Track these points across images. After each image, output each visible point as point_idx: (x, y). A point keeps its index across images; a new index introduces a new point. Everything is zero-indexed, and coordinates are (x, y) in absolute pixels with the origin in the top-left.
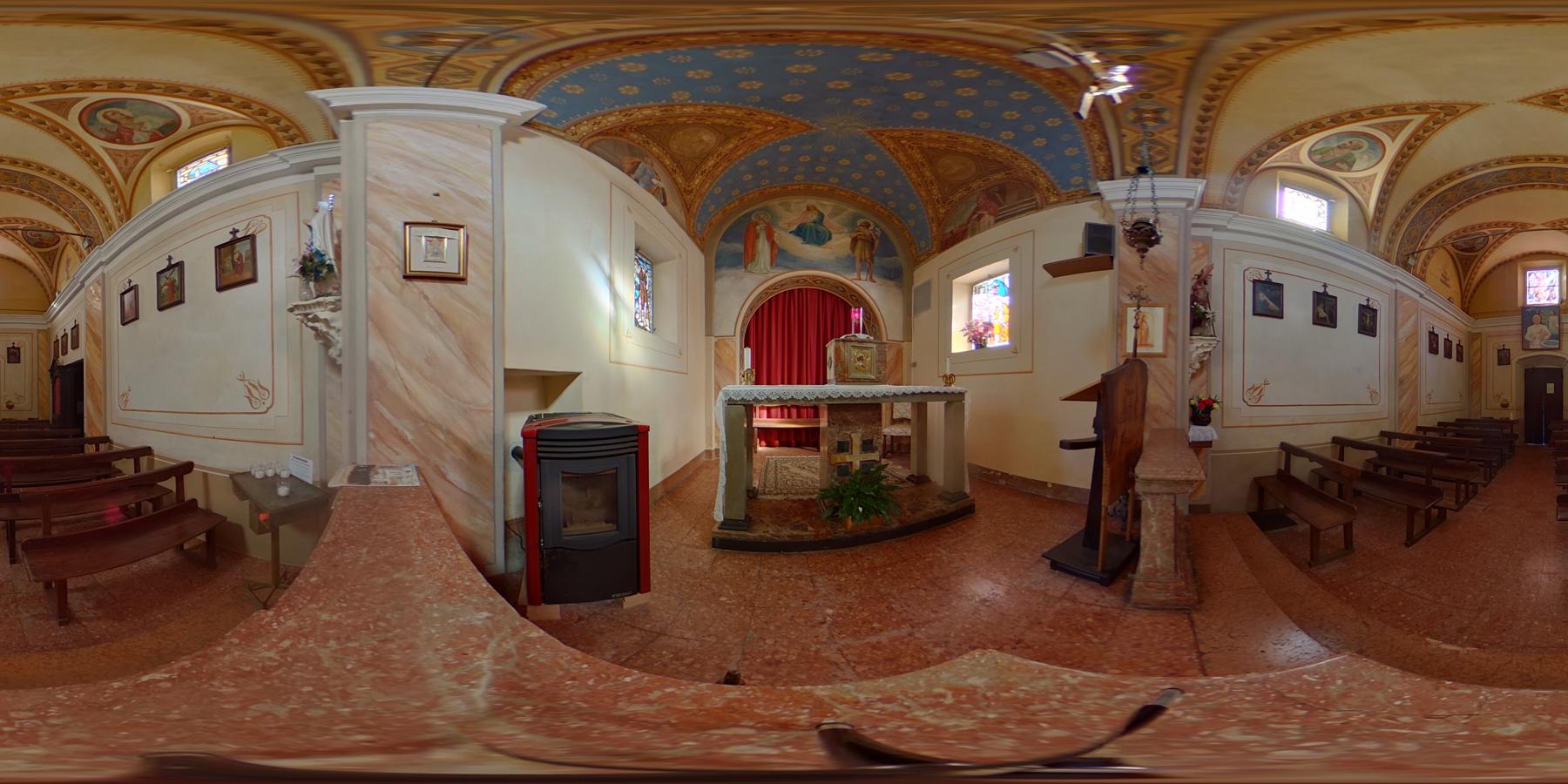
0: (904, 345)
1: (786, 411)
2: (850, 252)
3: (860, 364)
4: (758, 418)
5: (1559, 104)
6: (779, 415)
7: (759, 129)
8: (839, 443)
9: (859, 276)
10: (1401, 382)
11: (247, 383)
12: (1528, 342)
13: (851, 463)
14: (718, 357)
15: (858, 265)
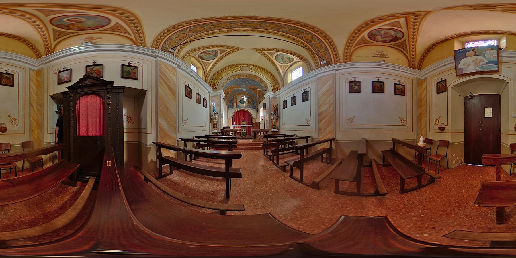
0: (256, 119)
5: (236, 48)
10: (320, 114)
11: (10, 117)
12: (462, 69)
14: (229, 122)
15: (249, 107)
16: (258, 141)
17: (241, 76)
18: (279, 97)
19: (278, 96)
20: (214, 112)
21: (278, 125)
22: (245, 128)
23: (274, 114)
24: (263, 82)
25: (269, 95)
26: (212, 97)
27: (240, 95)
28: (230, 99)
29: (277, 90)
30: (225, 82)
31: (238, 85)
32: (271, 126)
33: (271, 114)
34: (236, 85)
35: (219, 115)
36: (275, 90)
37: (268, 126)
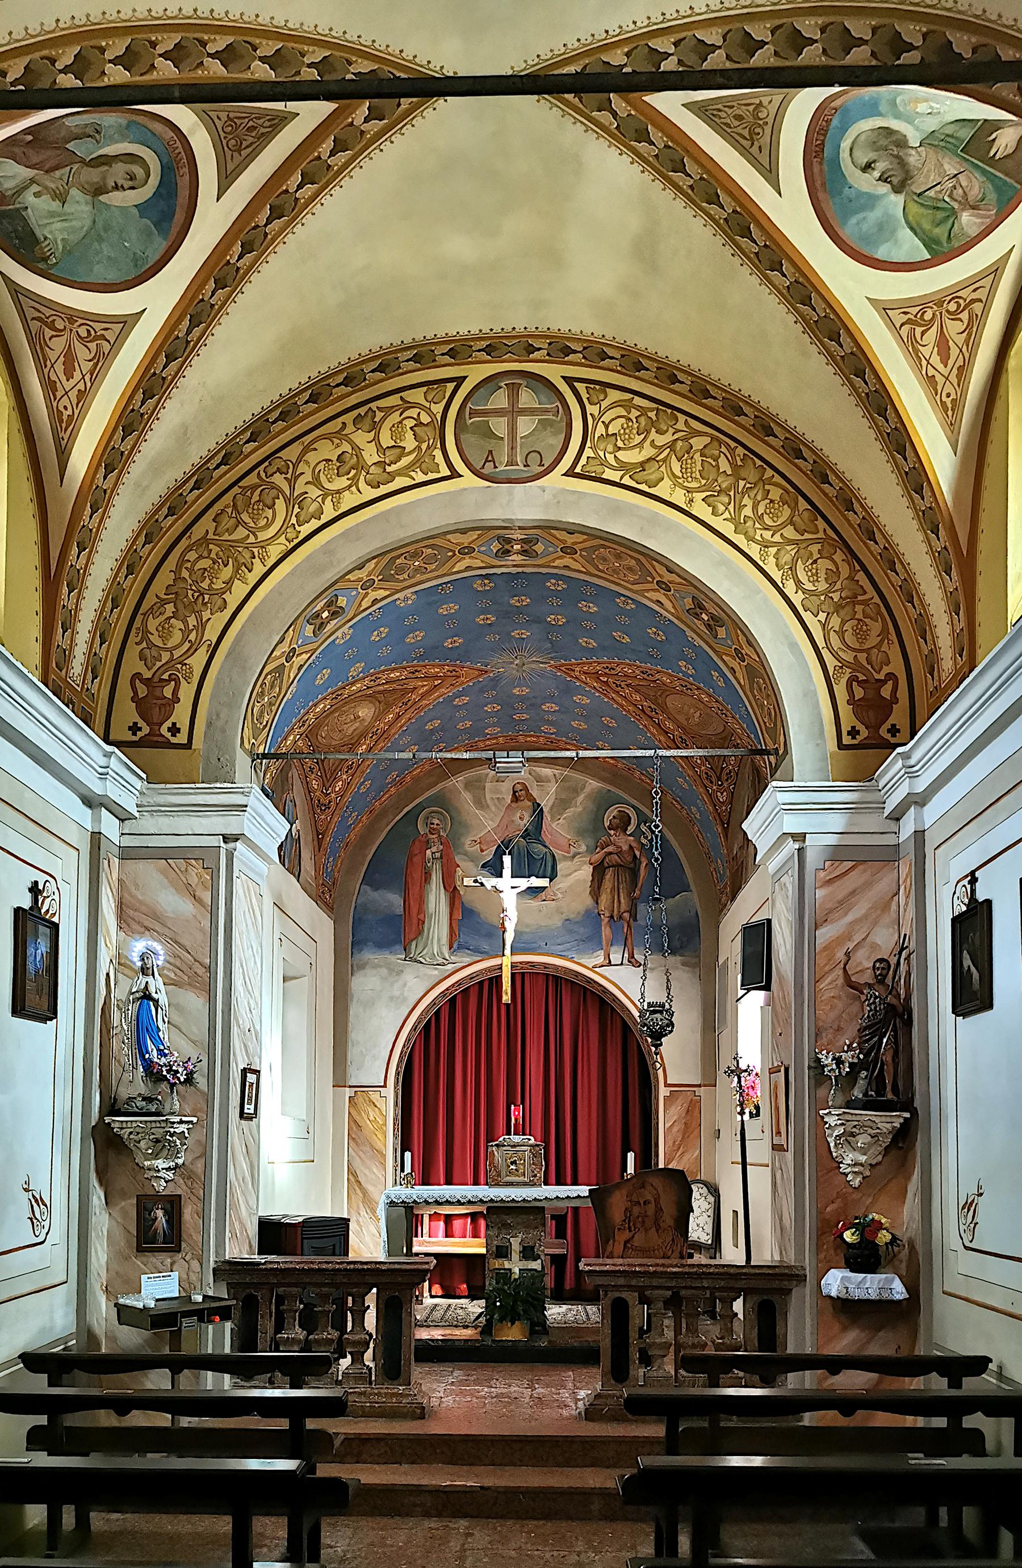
2: (589, 901)
4: (426, 1238)
7: (424, 686)
8: (497, 1247)
9: (608, 956)
15: (606, 932)
17: (467, 551)
18: (919, 835)
19: (908, 827)
20: (149, 1067)
25: (792, 824)
26: (126, 854)
28: (370, 831)
29: (903, 724)
30: (284, 648)
31: (462, 655)
34: (431, 652)
35: (209, 1099)
36: (874, 728)
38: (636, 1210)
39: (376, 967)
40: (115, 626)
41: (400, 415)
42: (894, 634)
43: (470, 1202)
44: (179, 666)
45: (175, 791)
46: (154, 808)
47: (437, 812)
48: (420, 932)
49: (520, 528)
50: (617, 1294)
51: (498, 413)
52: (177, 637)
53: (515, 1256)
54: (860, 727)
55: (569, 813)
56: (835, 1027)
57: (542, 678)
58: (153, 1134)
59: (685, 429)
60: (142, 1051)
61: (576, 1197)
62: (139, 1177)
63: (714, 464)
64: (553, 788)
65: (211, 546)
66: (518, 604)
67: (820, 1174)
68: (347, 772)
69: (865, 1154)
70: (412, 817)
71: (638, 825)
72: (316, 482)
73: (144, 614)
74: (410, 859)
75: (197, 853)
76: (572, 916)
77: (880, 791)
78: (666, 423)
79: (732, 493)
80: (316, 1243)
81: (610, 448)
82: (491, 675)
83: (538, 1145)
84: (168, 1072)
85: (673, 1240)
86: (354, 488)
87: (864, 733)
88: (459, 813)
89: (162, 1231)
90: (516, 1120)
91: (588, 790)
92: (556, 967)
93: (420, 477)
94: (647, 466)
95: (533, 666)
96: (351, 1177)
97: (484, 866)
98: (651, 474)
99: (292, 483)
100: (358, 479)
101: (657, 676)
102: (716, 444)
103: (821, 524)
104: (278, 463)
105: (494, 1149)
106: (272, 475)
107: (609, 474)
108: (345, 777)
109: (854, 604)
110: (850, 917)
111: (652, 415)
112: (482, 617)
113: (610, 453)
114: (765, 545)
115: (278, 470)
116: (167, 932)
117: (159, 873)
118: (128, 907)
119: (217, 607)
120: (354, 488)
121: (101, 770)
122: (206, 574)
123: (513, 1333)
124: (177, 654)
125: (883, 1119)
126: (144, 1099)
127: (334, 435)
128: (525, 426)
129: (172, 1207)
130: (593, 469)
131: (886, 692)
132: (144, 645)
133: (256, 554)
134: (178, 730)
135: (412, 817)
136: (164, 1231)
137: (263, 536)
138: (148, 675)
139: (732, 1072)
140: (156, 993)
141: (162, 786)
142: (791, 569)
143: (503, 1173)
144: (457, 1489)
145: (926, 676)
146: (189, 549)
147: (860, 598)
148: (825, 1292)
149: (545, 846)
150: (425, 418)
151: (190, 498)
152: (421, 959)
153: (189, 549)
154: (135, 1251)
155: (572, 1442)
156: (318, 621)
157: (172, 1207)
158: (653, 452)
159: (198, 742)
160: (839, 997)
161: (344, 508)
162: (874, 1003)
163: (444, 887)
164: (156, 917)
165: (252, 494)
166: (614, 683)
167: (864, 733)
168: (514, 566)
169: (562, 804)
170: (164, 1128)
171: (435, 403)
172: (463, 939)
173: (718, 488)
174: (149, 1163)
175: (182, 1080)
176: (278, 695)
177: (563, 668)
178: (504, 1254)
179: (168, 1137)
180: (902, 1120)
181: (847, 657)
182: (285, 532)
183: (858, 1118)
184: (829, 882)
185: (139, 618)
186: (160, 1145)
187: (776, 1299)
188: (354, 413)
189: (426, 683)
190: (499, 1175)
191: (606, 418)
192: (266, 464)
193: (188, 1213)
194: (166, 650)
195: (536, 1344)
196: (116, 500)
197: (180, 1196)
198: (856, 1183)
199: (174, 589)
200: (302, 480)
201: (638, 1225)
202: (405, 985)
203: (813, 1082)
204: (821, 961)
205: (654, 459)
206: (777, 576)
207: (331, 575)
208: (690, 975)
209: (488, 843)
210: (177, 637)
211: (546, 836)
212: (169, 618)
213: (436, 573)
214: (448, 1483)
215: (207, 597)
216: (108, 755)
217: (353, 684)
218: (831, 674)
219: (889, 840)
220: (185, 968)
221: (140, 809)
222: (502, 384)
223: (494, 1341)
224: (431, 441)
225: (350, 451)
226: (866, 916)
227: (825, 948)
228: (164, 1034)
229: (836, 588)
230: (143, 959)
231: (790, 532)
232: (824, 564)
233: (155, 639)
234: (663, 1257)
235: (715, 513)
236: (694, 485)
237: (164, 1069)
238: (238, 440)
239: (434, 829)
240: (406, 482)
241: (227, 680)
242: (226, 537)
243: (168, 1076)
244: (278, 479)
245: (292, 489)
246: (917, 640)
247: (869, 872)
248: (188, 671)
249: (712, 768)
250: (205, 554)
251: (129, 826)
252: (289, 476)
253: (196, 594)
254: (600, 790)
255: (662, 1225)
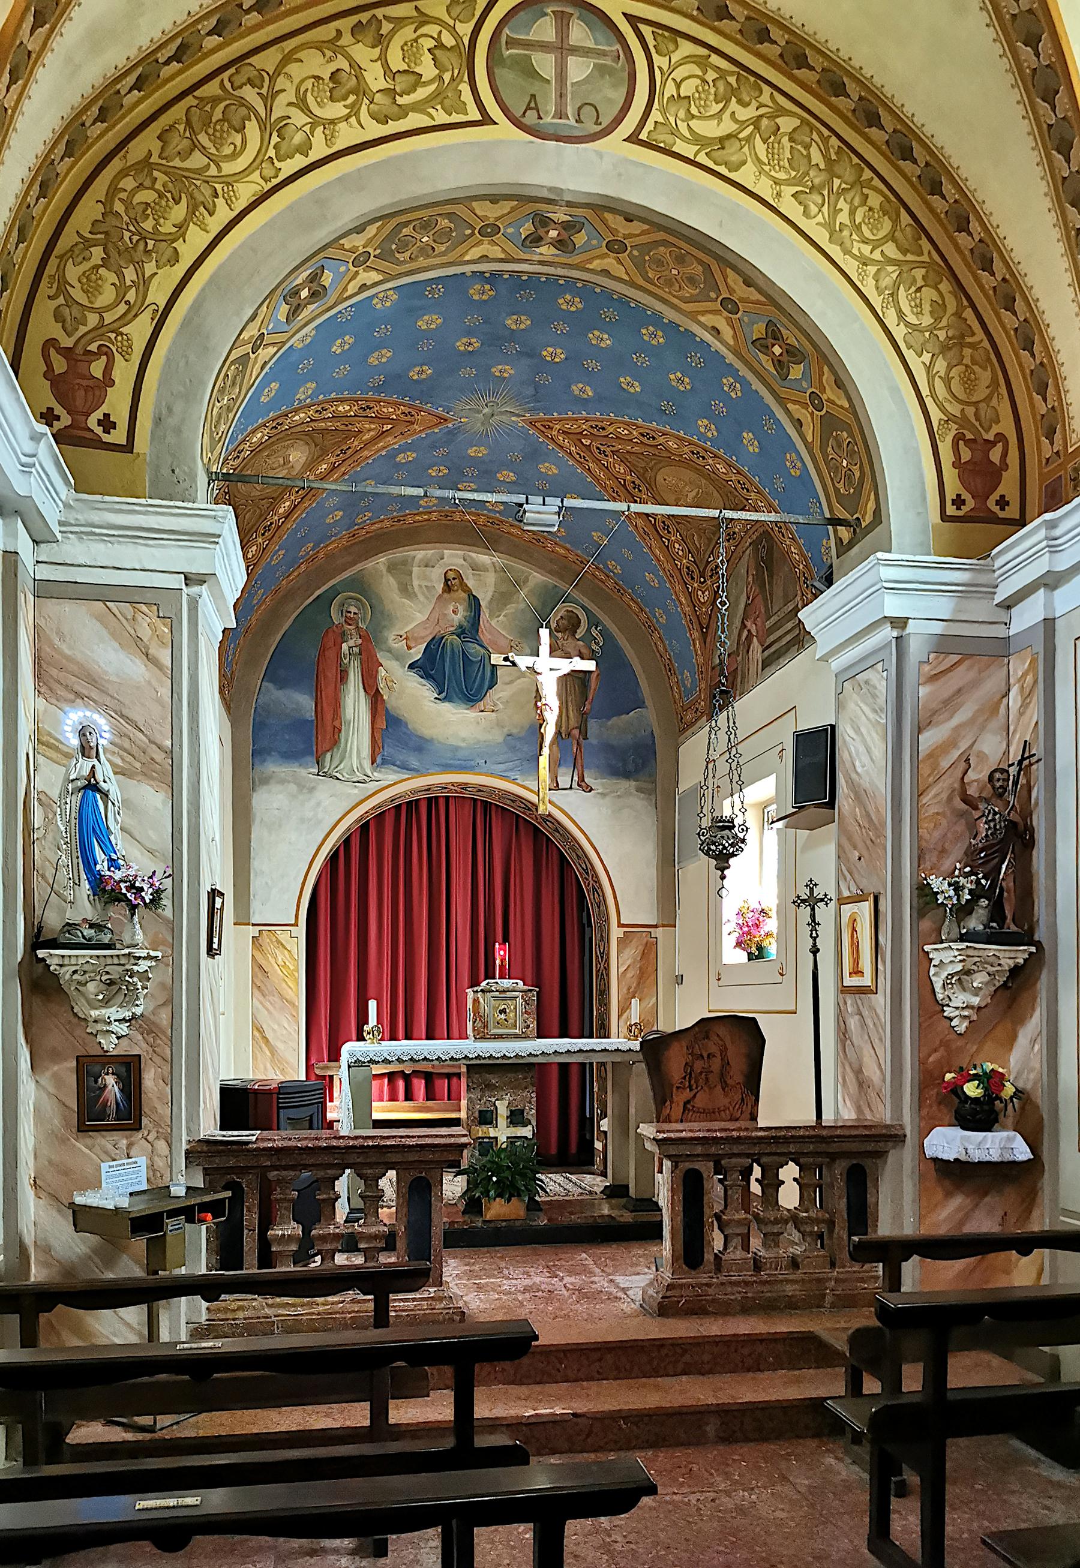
1: (401, 1084)
3: (503, 1016)
6: (386, 1096)
7: (370, 429)
8: (480, 1112)
13: (496, 1138)
16: (736, 1294)
17: (490, 231)
18: (1049, 624)
21: (1037, 1063)
22: (515, 1087)
23: (964, 911)
24: (796, 372)
25: (893, 606)
26: (45, 590)
27: (421, 554)
30: (252, 331)
31: (426, 391)
32: (928, 1079)
33: (920, 912)
35: (174, 927)
36: (981, 497)
37: (872, 1072)
38: (698, 1065)
39: (282, 782)
40: (20, 268)
41: (415, 32)
42: (1004, 387)
43: (386, 1061)
44: (113, 335)
45: (117, 506)
46: (83, 529)
47: (358, 600)
48: (335, 742)
49: (570, 204)
50: (688, 1165)
51: (544, 47)
52: (107, 295)
53: (502, 1122)
54: (966, 496)
55: (511, 609)
56: (940, 849)
57: (508, 435)
58: (107, 973)
59: (771, 104)
60: (89, 863)
61: (602, 1051)
62: (78, 1032)
63: (805, 153)
64: (491, 578)
65: (156, 173)
66: (514, 327)
67: (922, 1019)
68: (263, 534)
69: (977, 995)
70: (324, 602)
71: (589, 630)
72: (301, 104)
73: (61, 257)
74: (323, 650)
75: (149, 596)
76: (515, 731)
77: (994, 571)
78: (748, 94)
79: (826, 193)
80: (293, 1113)
81: (682, 114)
82: (450, 425)
83: (531, 991)
84: (128, 889)
85: (743, 1100)
86: (353, 120)
87: (970, 504)
88: (381, 601)
89: (114, 1102)
90: (502, 961)
91: (531, 584)
92: (492, 790)
93: (442, 118)
94: (727, 144)
95: (504, 418)
96: (256, 1033)
97: (412, 666)
98: (732, 154)
99: (268, 100)
100: (359, 109)
101: (661, 440)
102: (807, 129)
103: (924, 243)
104: (248, 72)
105: (479, 995)
106: (240, 87)
107: (680, 147)
108: (260, 540)
109: (962, 345)
110: (955, 721)
111: (732, 80)
112: (465, 340)
113: (683, 121)
114: (865, 262)
115: (250, 82)
116: (108, 701)
117: (94, 621)
118: (49, 664)
119: (164, 259)
120: (353, 120)
121: (24, 459)
122: (149, 211)
123: (497, 1209)
124: (109, 318)
125: (1008, 955)
126: (91, 926)
127: (326, 45)
128: (578, 69)
129: (128, 1071)
130: (661, 137)
131: (995, 455)
132: (61, 300)
133: (220, 192)
134: (114, 425)
135: (324, 602)
136: (117, 1104)
137: (228, 168)
138: (67, 342)
139: (804, 901)
140: (105, 781)
141: (98, 497)
142: (892, 295)
143: (491, 1025)
144: (544, 1420)
145: (1039, 441)
146: (123, 173)
147: (969, 340)
148: (929, 1153)
149: (482, 646)
150: (448, 40)
151: (128, 101)
152: (338, 775)
153: (123, 173)
154: (75, 1130)
155: (662, 1346)
156: (295, 301)
157: (128, 1071)
158: (733, 127)
159: (142, 443)
160: (943, 814)
161: (340, 145)
162: (994, 820)
163: (364, 688)
164: (93, 681)
165: (213, 108)
166: (598, 448)
167: (970, 504)
168: (541, 263)
169: (502, 598)
170: (123, 965)
171: (460, 21)
172: (388, 750)
173: (809, 183)
174: (97, 1012)
175: (148, 901)
176: (238, 397)
177: (538, 425)
178: (489, 1120)
179: (127, 978)
180: (1026, 956)
181: (954, 409)
182: (260, 167)
183: (980, 953)
184: (933, 678)
185: (53, 262)
186: (115, 988)
187: (867, 1163)
188: (353, 20)
189: (373, 426)
190: (485, 1026)
191: (678, 74)
192: (233, 70)
193: (150, 1079)
194: (93, 310)
195: (534, 1223)
196: (40, 73)
197: (139, 1056)
198: (962, 1029)
199: (103, 228)
200: (281, 100)
201: (701, 1082)
202: (318, 804)
203: (915, 915)
204: (925, 770)
205: (736, 136)
206: (876, 301)
207: (323, 235)
208: (645, 803)
209: (415, 639)
210: (107, 295)
211: (485, 636)
212: (96, 267)
213: (444, 259)
214: (532, 1412)
215: (151, 243)
216: (36, 438)
217: (296, 411)
218: (935, 429)
219: (999, 631)
220: (135, 750)
221: (63, 529)
222: (549, 11)
223: (484, 1222)
224: (456, 71)
225: (347, 69)
226: (972, 721)
227: (930, 755)
228: (116, 838)
229: (940, 325)
230: (84, 735)
231: (891, 250)
232: (928, 293)
233: (77, 294)
234: (731, 1120)
235: (806, 213)
236: (782, 176)
237: (123, 885)
238: (200, 27)
239: (351, 619)
240: (423, 121)
241: (182, 364)
242: (177, 163)
243: (129, 895)
244: (249, 94)
245: (269, 110)
246: (1031, 399)
247: (976, 668)
248: (125, 343)
249: (694, 562)
250: (147, 183)
251: (46, 552)
252: (264, 91)
253: (135, 238)
254: (545, 586)
255: (730, 1082)
